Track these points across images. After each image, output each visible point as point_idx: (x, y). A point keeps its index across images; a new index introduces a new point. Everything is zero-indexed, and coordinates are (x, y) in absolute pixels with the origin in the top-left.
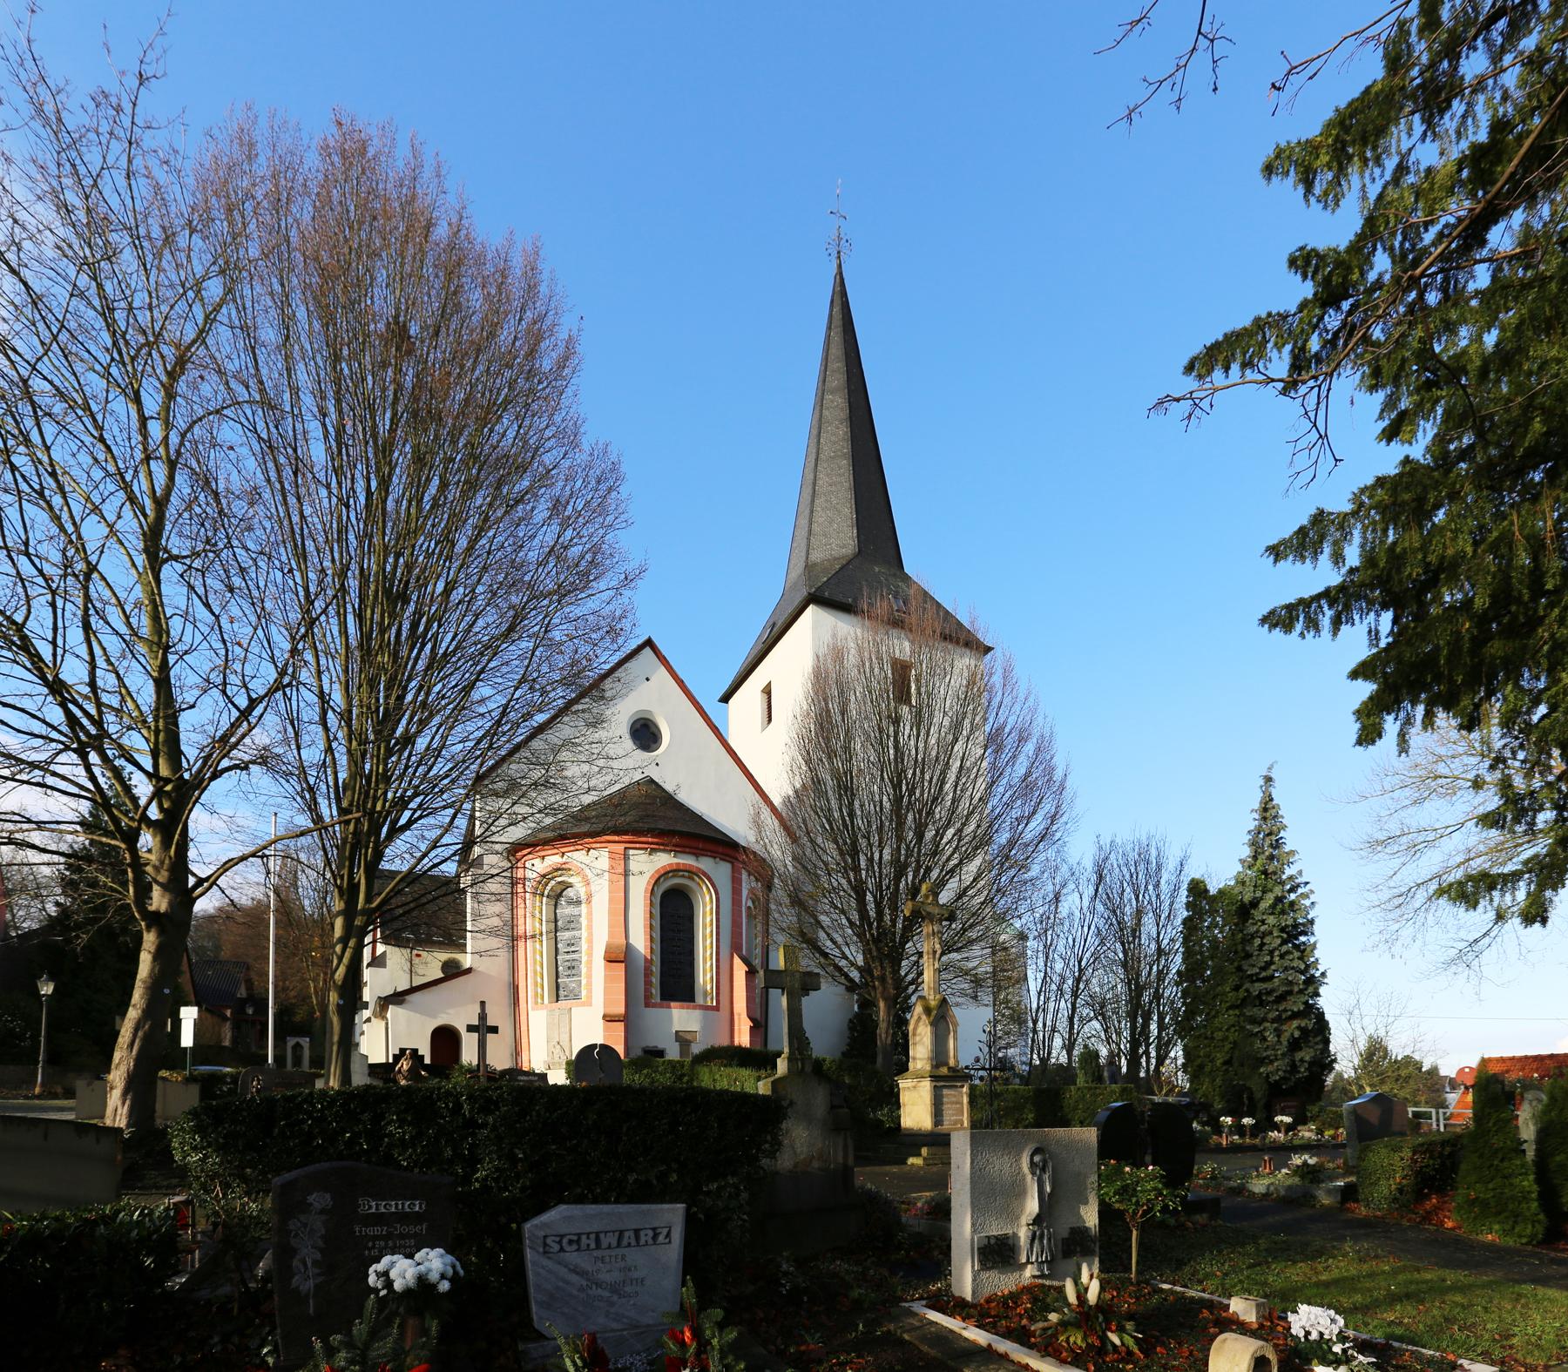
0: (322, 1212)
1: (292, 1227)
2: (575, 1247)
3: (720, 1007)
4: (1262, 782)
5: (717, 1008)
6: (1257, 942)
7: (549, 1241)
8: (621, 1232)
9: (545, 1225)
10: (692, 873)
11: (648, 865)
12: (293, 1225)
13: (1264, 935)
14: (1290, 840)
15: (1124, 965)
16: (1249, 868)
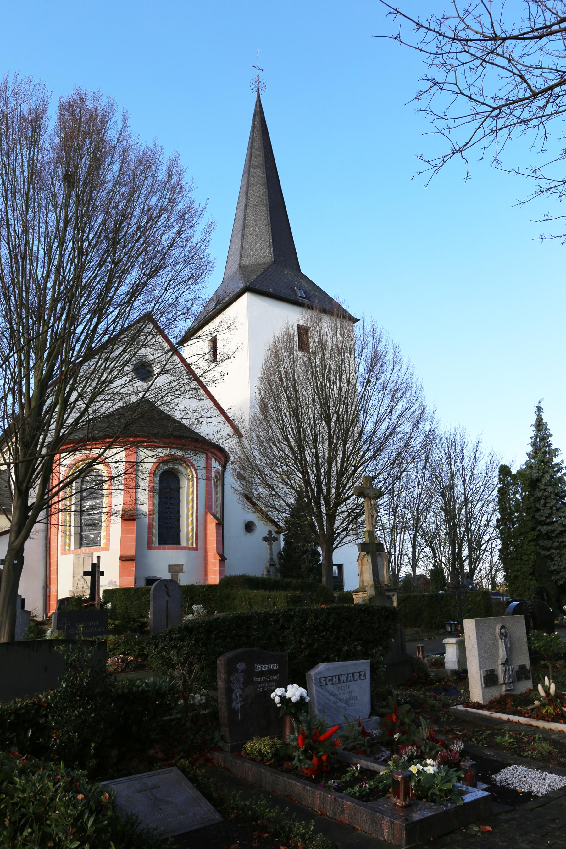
0: (242, 671)
1: (232, 679)
2: (331, 683)
3: (200, 546)
4: (536, 410)
5: (196, 549)
6: (543, 501)
7: (322, 680)
8: (348, 674)
9: (320, 673)
10: (173, 459)
11: (149, 457)
12: (232, 678)
13: (546, 498)
14: (555, 442)
15: (445, 510)
16: (533, 458)
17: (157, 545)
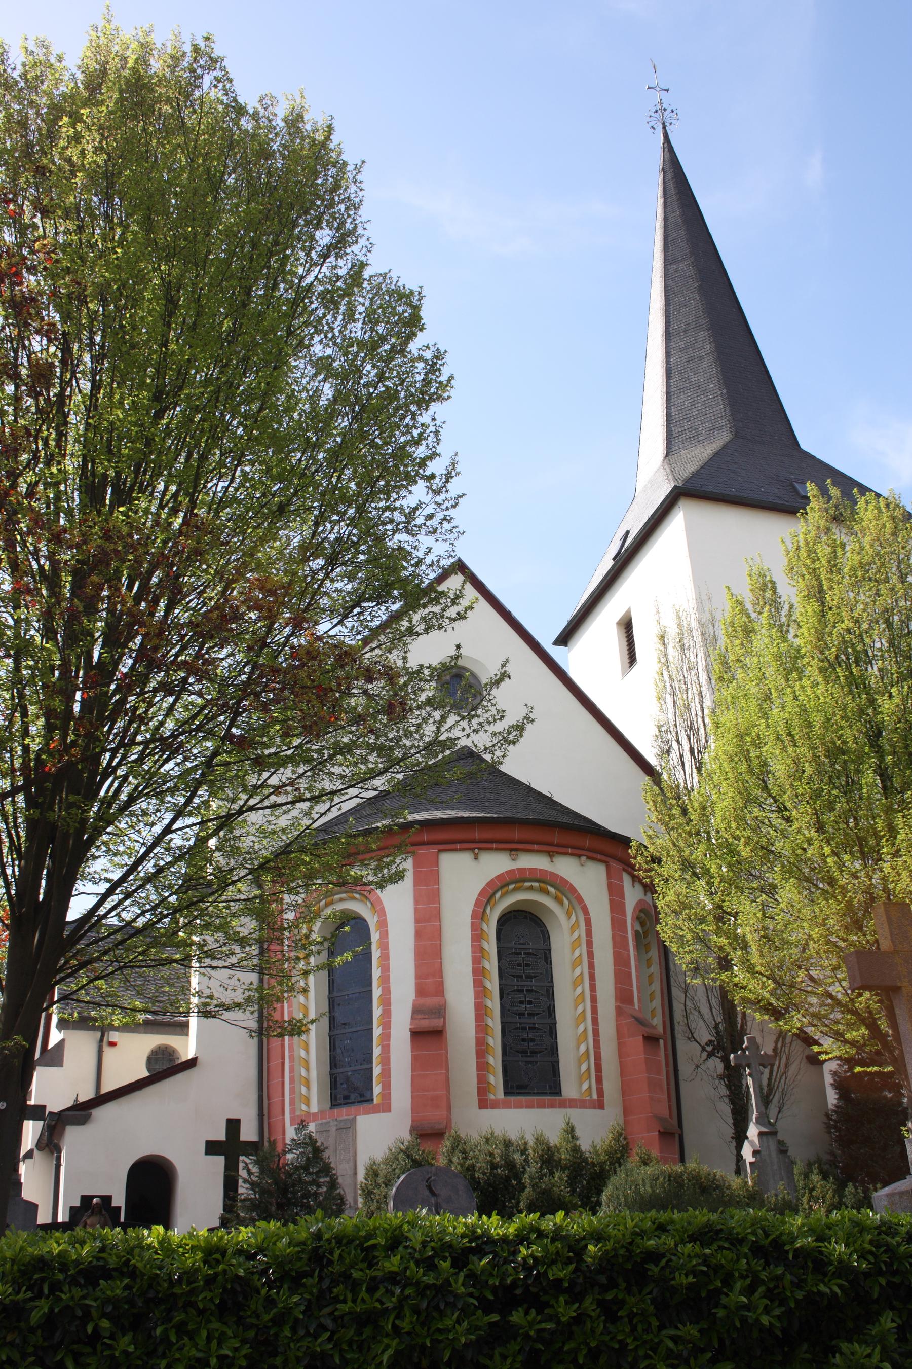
11: (465, 877)
17: (500, 1094)
